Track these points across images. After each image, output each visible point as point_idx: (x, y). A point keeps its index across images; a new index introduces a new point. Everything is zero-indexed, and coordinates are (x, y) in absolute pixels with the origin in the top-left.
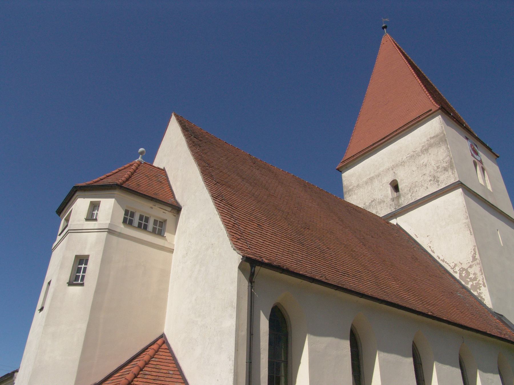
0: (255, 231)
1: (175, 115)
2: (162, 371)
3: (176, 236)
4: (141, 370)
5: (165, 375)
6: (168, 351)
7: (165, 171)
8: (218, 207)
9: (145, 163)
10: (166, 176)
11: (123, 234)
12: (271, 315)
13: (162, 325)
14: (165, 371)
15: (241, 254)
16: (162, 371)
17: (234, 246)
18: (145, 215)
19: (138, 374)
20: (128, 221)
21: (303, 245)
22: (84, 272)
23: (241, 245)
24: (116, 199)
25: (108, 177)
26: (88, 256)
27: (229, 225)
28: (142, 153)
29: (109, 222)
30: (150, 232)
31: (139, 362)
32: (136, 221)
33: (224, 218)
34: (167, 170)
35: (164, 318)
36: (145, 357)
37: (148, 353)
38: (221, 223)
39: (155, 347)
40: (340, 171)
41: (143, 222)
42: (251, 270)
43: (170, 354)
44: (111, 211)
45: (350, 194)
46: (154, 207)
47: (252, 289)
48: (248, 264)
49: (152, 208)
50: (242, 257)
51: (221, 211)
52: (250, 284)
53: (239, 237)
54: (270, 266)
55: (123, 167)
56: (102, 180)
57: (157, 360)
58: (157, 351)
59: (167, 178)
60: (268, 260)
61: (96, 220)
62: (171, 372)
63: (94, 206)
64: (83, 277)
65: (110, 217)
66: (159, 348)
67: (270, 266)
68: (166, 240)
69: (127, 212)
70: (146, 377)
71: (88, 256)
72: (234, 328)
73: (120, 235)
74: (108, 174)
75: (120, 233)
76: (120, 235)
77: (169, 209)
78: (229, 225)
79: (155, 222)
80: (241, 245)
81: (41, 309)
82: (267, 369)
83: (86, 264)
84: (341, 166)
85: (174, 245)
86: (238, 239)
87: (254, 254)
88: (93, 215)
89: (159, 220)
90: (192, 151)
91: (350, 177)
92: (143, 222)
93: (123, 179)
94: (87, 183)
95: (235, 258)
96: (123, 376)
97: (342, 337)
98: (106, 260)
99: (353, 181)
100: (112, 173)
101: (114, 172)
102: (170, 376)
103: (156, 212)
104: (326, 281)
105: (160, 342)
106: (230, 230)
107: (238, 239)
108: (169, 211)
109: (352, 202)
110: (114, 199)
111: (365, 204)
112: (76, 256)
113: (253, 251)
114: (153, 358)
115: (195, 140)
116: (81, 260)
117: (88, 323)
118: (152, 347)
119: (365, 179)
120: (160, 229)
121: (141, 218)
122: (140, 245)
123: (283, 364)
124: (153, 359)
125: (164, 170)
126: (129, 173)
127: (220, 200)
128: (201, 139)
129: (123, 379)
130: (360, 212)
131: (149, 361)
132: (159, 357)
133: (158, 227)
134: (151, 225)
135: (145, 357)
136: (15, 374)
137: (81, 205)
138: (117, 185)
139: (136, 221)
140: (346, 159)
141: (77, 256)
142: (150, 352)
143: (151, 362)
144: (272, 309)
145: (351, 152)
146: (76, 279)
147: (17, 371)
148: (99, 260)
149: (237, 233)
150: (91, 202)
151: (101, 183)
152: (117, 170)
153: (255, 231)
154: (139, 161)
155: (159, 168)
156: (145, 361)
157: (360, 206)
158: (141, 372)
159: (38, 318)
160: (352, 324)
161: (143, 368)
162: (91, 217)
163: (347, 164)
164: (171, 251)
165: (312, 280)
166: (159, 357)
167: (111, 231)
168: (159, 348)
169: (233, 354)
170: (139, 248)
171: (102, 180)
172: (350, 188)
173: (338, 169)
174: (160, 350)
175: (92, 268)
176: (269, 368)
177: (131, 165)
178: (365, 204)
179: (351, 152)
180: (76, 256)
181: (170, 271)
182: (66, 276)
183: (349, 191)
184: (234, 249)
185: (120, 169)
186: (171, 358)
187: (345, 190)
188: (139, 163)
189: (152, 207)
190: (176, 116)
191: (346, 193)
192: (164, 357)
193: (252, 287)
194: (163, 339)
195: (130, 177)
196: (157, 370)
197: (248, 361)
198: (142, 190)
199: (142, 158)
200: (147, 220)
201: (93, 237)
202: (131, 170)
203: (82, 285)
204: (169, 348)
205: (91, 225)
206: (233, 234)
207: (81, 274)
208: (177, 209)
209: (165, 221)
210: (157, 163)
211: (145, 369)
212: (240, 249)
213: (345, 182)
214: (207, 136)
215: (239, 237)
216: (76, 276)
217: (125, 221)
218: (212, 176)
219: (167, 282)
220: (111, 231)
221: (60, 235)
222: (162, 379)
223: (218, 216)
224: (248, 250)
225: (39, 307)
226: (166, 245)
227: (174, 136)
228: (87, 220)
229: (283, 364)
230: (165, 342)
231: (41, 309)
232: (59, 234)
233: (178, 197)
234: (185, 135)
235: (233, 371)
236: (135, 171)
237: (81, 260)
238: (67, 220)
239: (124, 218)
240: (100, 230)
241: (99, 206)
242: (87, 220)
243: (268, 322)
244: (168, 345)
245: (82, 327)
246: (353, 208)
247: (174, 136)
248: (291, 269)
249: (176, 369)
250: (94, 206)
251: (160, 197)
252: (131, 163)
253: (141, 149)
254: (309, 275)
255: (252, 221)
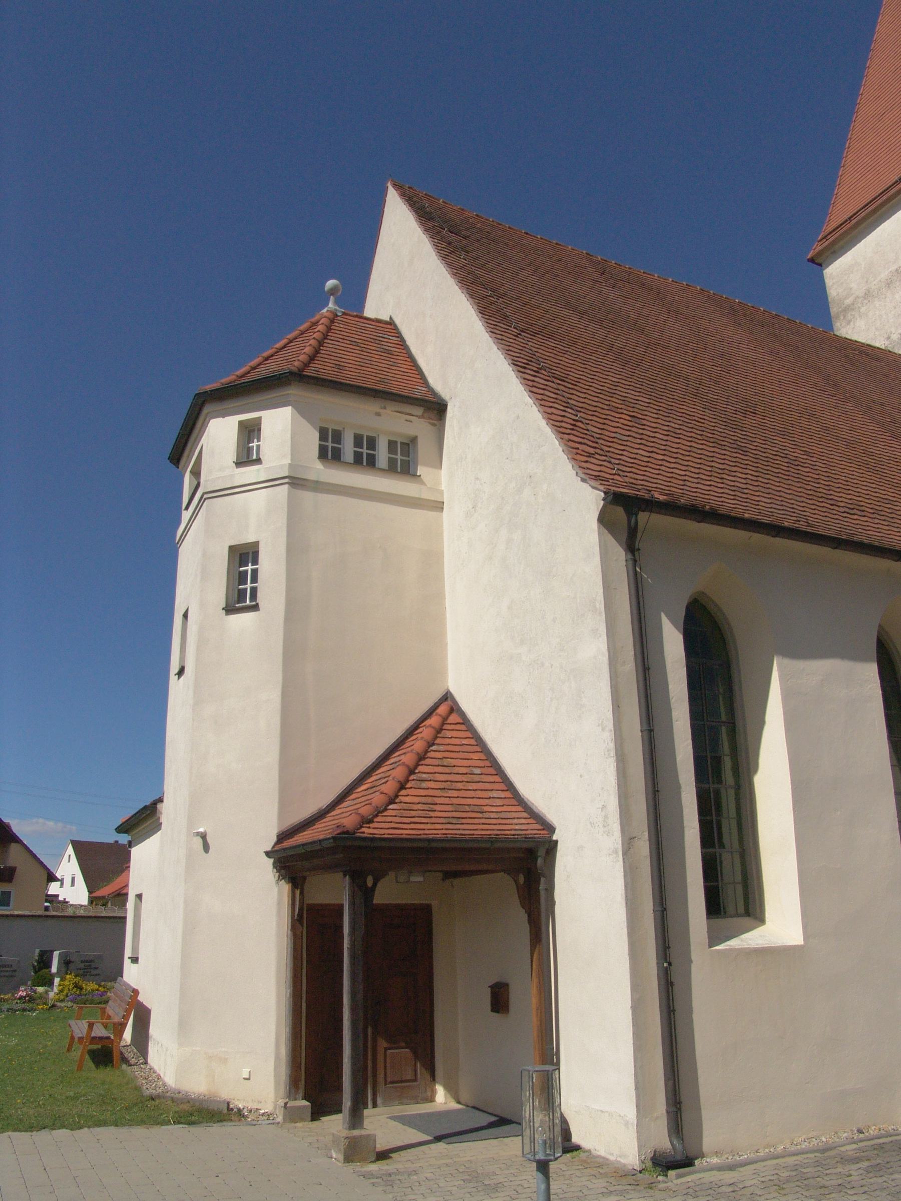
0: (628, 433)
1: (395, 186)
2: (456, 770)
3: (444, 471)
4: (412, 772)
5: (465, 778)
6: (463, 727)
7: (395, 325)
8: (532, 388)
9: (344, 314)
10: (399, 336)
11: (323, 483)
12: (685, 623)
13: (442, 672)
14: (464, 770)
15: (602, 487)
16: (456, 770)
17: (580, 471)
18: (366, 433)
19: (407, 781)
20: (330, 452)
21: (745, 452)
22: (255, 579)
23: (599, 468)
24: (295, 407)
25: (267, 359)
26: (256, 544)
27: (563, 424)
28: (333, 291)
29: (287, 461)
30: (384, 470)
31: (406, 757)
32: (348, 449)
33: (549, 410)
34: (398, 321)
35: (444, 658)
36: (417, 744)
37: (419, 736)
38: (543, 423)
39: (434, 721)
40: (818, 262)
41: (365, 451)
42: (629, 520)
43: (469, 734)
44: (289, 435)
45: (849, 317)
46: (381, 411)
47: (635, 566)
48: (620, 511)
49: (378, 414)
50: (602, 495)
51: (540, 397)
52: (630, 556)
53: (592, 451)
54: (671, 508)
55: (297, 332)
56: (255, 368)
57: (441, 748)
58: (439, 730)
59: (403, 340)
60: (667, 495)
61: (258, 461)
62: (478, 771)
63: (250, 431)
64: (254, 591)
65: (287, 449)
66: (443, 724)
67: (671, 508)
68: (423, 483)
69: (323, 434)
70: (424, 785)
71: (256, 544)
72: (605, 659)
73: (318, 487)
74: (266, 354)
75: (317, 482)
76: (318, 487)
77: (419, 411)
78: (563, 424)
79: (392, 445)
80: (599, 468)
81: (181, 672)
82: (690, 742)
83: (255, 562)
84: (819, 248)
85: (442, 492)
86: (590, 455)
87: (631, 485)
88: (249, 450)
89: (399, 440)
90: (449, 265)
91: (843, 274)
92: (365, 451)
93: (303, 358)
94: (224, 381)
95: (589, 500)
96: (375, 789)
97: (857, 657)
98: (296, 550)
99: (854, 285)
100: (274, 350)
101: (278, 345)
102: (476, 778)
103: (390, 423)
104: (809, 530)
105: (443, 709)
106: (566, 437)
107: (590, 455)
108: (419, 417)
109: (855, 337)
110: (290, 408)
111: (888, 338)
112: (230, 547)
113: (627, 479)
114: (433, 744)
115: (453, 237)
116: (244, 556)
117: (283, 687)
118: (427, 722)
119: (884, 275)
120: (404, 460)
121: (358, 440)
122: (366, 503)
123: (724, 729)
124: (434, 748)
125: (391, 323)
126: (312, 342)
127: (535, 370)
128: (467, 233)
129: (377, 794)
130: (878, 359)
131: (426, 752)
132: (448, 741)
133: (399, 457)
134: (382, 455)
135: (417, 744)
136: (159, 806)
137: (220, 433)
138: (291, 373)
139: (348, 449)
140: (830, 229)
141: (232, 549)
142: (425, 733)
143: (429, 755)
144: (688, 608)
145: (842, 208)
146: (240, 598)
147: (161, 800)
148: (282, 549)
149: (583, 437)
150: (241, 424)
151: (254, 376)
152: (285, 341)
153: (628, 433)
154: (331, 312)
155: (378, 321)
156: (418, 754)
157: (877, 345)
158: (412, 778)
159: (179, 693)
160: (880, 626)
161: (416, 768)
162: (246, 457)
163: (834, 242)
164: (438, 506)
165: (776, 530)
166: (448, 741)
167: (295, 482)
168: (443, 724)
169: (610, 716)
170: (364, 510)
171: (255, 368)
172: (848, 301)
173: (812, 260)
174: (445, 727)
175: (271, 569)
176: (693, 739)
177: (316, 324)
178: (888, 338)
179: (842, 208)
180: (230, 547)
181: (443, 553)
182: (218, 593)
183: (846, 310)
184: (583, 480)
185: (291, 336)
186: (473, 742)
187: (834, 310)
188: (331, 316)
189: (379, 411)
190: (398, 187)
191: (838, 317)
192: (457, 741)
193: (635, 561)
194: (449, 702)
195: (317, 352)
196: (447, 770)
197: (645, 727)
198: (349, 376)
199: (336, 302)
200: (372, 443)
201: (258, 500)
202: (315, 335)
203: (255, 608)
204: (465, 722)
205: (250, 474)
206: (577, 445)
207: (249, 585)
208: (436, 408)
209: (414, 440)
210: (371, 310)
211: (420, 768)
212: (596, 478)
213: (834, 290)
214: (479, 225)
215: (592, 451)
216: (239, 590)
217: (323, 454)
218: (505, 317)
219: (439, 578)
220: (295, 482)
221: (187, 508)
222: (459, 786)
223: (535, 409)
224: (616, 477)
225: (174, 668)
226: (426, 495)
227: (401, 234)
228: (239, 464)
229: (724, 729)
230: (455, 708)
231: (181, 672)
232: (184, 507)
233: (435, 381)
234: (427, 230)
235: (613, 753)
236: (325, 336)
237: (244, 556)
238: (196, 473)
239: (320, 446)
240: (272, 482)
241: (259, 430)
242: (239, 464)
243: (681, 636)
244: (462, 714)
245: (272, 696)
246: (861, 352)
247: (401, 234)
248: (722, 511)
249: (488, 763)
250: (250, 431)
251: (395, 387)
252: (314, 320)
253: (331, 283)
254: (766, 520)
255: (615, 409)
